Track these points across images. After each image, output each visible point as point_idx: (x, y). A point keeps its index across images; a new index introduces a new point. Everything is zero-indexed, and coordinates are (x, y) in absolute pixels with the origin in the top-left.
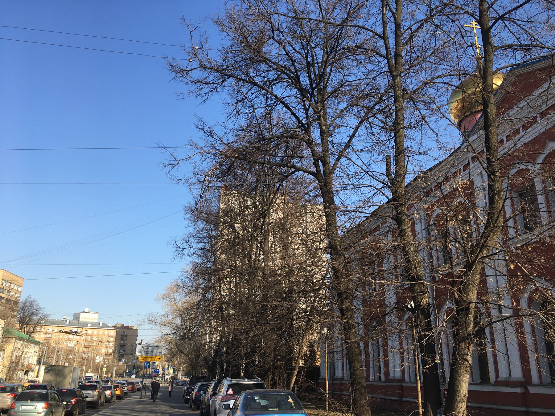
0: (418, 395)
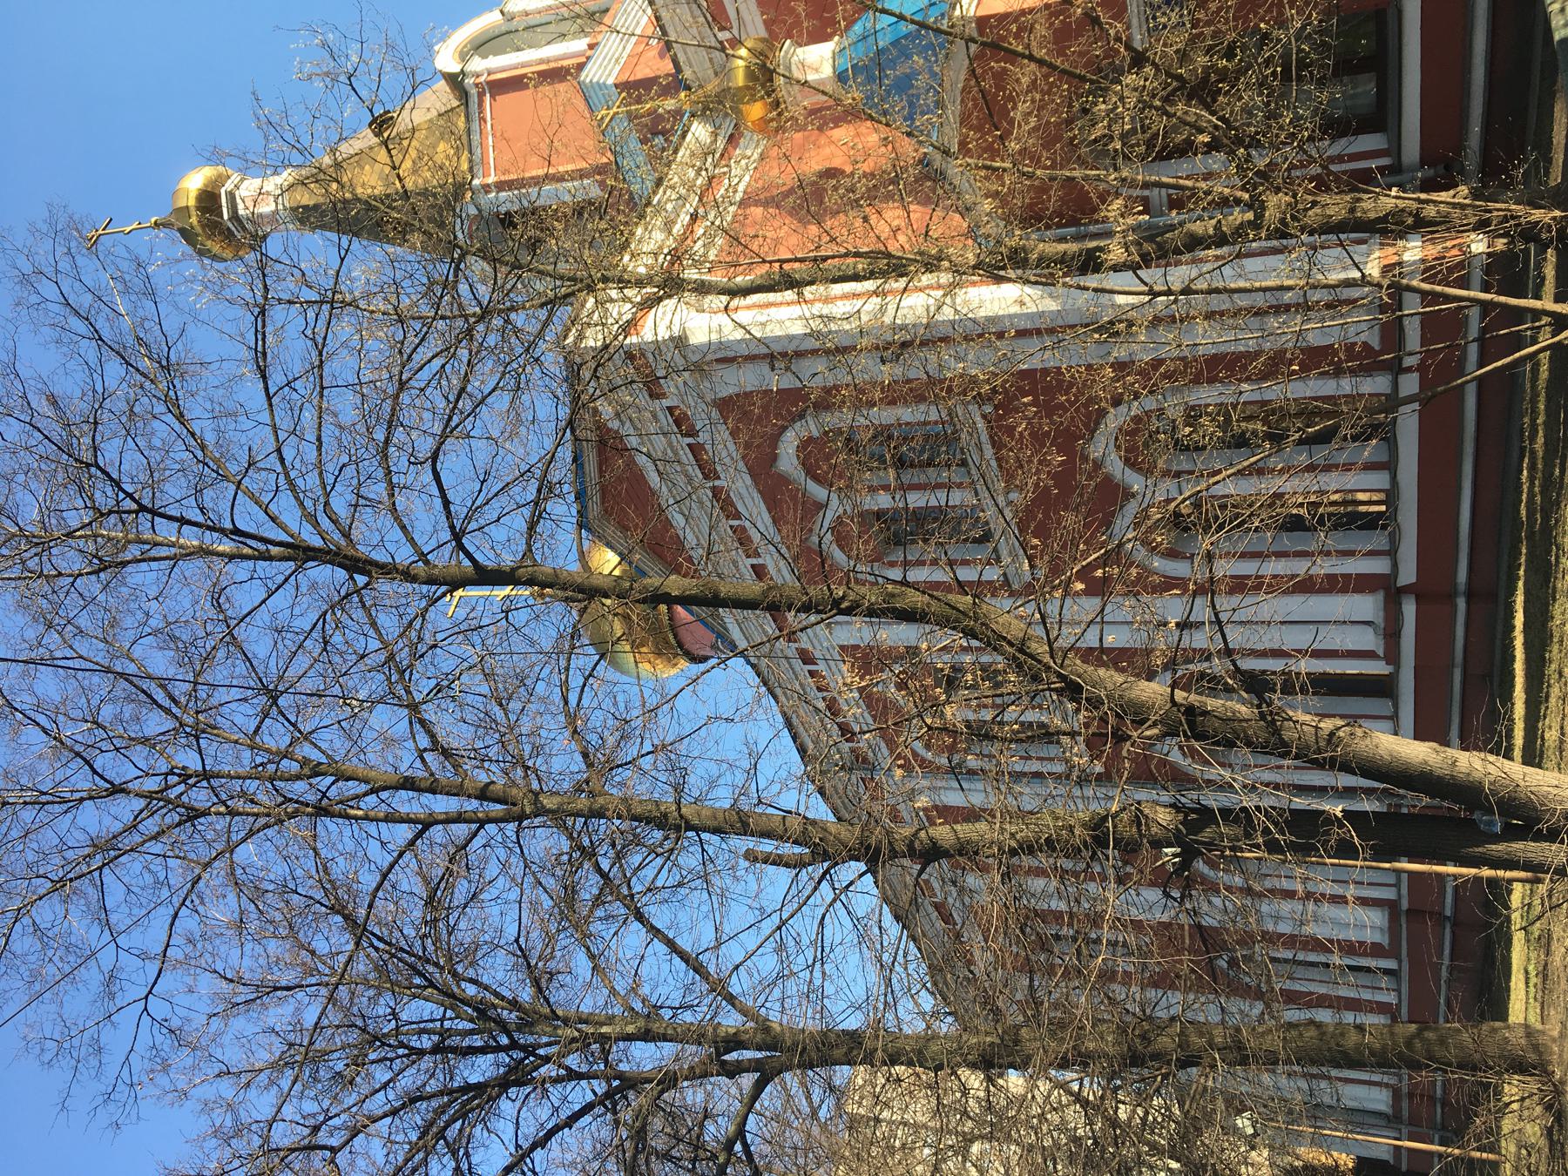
0: (1438, 875)
